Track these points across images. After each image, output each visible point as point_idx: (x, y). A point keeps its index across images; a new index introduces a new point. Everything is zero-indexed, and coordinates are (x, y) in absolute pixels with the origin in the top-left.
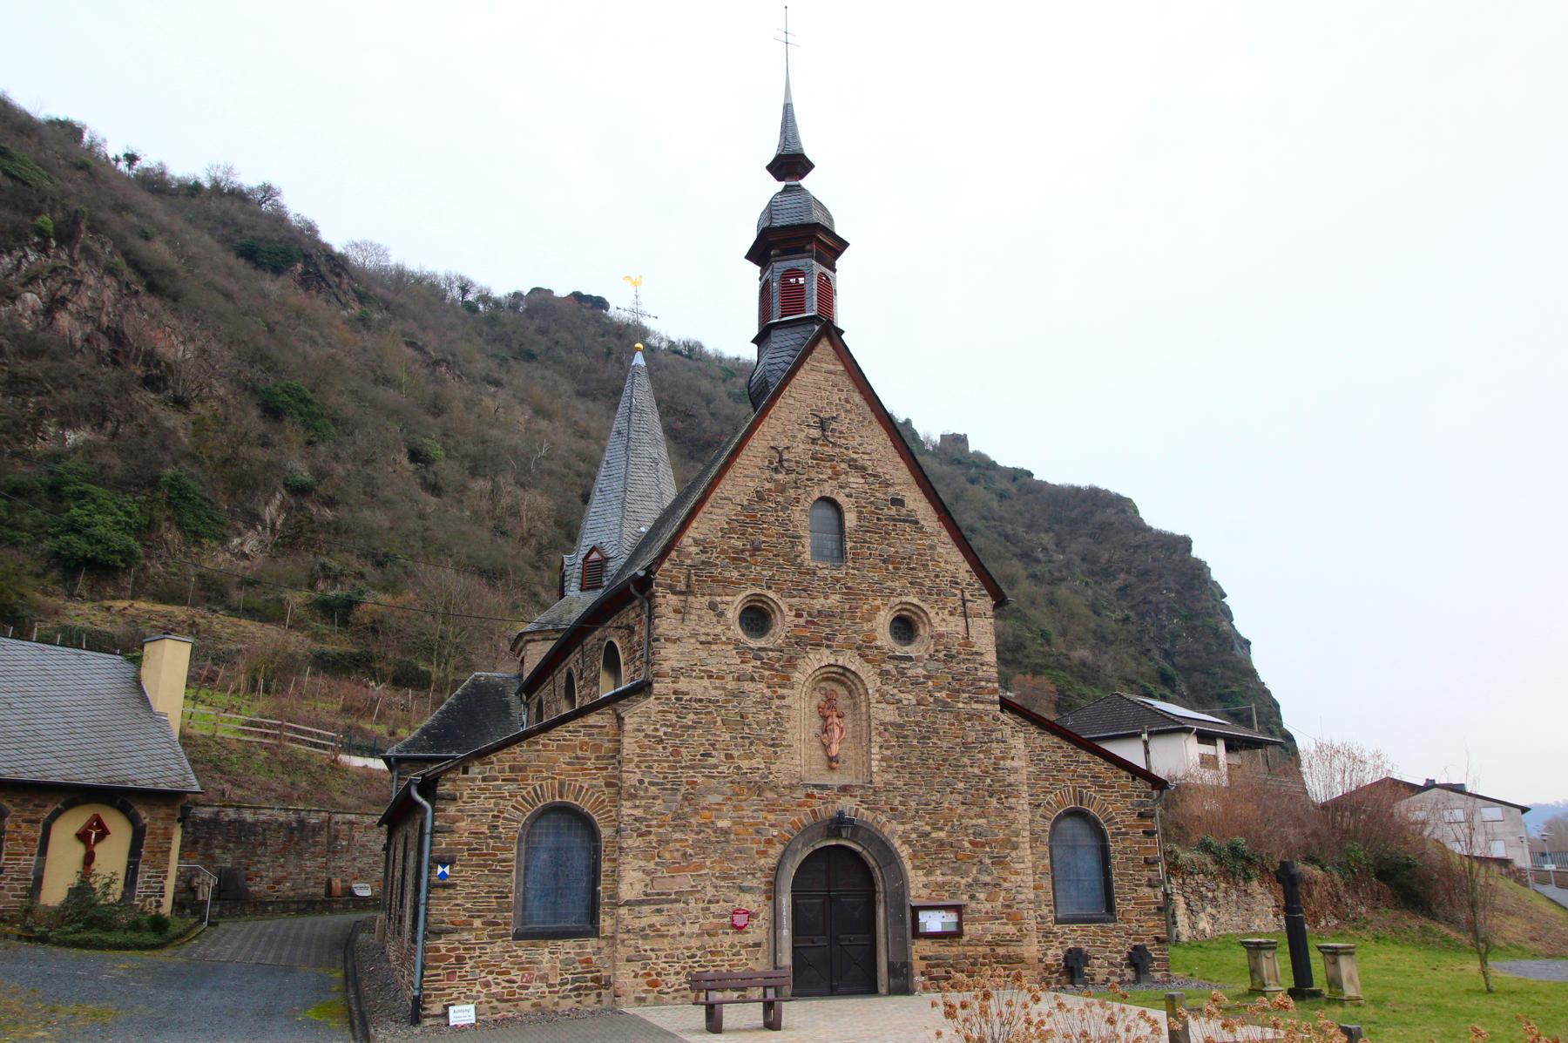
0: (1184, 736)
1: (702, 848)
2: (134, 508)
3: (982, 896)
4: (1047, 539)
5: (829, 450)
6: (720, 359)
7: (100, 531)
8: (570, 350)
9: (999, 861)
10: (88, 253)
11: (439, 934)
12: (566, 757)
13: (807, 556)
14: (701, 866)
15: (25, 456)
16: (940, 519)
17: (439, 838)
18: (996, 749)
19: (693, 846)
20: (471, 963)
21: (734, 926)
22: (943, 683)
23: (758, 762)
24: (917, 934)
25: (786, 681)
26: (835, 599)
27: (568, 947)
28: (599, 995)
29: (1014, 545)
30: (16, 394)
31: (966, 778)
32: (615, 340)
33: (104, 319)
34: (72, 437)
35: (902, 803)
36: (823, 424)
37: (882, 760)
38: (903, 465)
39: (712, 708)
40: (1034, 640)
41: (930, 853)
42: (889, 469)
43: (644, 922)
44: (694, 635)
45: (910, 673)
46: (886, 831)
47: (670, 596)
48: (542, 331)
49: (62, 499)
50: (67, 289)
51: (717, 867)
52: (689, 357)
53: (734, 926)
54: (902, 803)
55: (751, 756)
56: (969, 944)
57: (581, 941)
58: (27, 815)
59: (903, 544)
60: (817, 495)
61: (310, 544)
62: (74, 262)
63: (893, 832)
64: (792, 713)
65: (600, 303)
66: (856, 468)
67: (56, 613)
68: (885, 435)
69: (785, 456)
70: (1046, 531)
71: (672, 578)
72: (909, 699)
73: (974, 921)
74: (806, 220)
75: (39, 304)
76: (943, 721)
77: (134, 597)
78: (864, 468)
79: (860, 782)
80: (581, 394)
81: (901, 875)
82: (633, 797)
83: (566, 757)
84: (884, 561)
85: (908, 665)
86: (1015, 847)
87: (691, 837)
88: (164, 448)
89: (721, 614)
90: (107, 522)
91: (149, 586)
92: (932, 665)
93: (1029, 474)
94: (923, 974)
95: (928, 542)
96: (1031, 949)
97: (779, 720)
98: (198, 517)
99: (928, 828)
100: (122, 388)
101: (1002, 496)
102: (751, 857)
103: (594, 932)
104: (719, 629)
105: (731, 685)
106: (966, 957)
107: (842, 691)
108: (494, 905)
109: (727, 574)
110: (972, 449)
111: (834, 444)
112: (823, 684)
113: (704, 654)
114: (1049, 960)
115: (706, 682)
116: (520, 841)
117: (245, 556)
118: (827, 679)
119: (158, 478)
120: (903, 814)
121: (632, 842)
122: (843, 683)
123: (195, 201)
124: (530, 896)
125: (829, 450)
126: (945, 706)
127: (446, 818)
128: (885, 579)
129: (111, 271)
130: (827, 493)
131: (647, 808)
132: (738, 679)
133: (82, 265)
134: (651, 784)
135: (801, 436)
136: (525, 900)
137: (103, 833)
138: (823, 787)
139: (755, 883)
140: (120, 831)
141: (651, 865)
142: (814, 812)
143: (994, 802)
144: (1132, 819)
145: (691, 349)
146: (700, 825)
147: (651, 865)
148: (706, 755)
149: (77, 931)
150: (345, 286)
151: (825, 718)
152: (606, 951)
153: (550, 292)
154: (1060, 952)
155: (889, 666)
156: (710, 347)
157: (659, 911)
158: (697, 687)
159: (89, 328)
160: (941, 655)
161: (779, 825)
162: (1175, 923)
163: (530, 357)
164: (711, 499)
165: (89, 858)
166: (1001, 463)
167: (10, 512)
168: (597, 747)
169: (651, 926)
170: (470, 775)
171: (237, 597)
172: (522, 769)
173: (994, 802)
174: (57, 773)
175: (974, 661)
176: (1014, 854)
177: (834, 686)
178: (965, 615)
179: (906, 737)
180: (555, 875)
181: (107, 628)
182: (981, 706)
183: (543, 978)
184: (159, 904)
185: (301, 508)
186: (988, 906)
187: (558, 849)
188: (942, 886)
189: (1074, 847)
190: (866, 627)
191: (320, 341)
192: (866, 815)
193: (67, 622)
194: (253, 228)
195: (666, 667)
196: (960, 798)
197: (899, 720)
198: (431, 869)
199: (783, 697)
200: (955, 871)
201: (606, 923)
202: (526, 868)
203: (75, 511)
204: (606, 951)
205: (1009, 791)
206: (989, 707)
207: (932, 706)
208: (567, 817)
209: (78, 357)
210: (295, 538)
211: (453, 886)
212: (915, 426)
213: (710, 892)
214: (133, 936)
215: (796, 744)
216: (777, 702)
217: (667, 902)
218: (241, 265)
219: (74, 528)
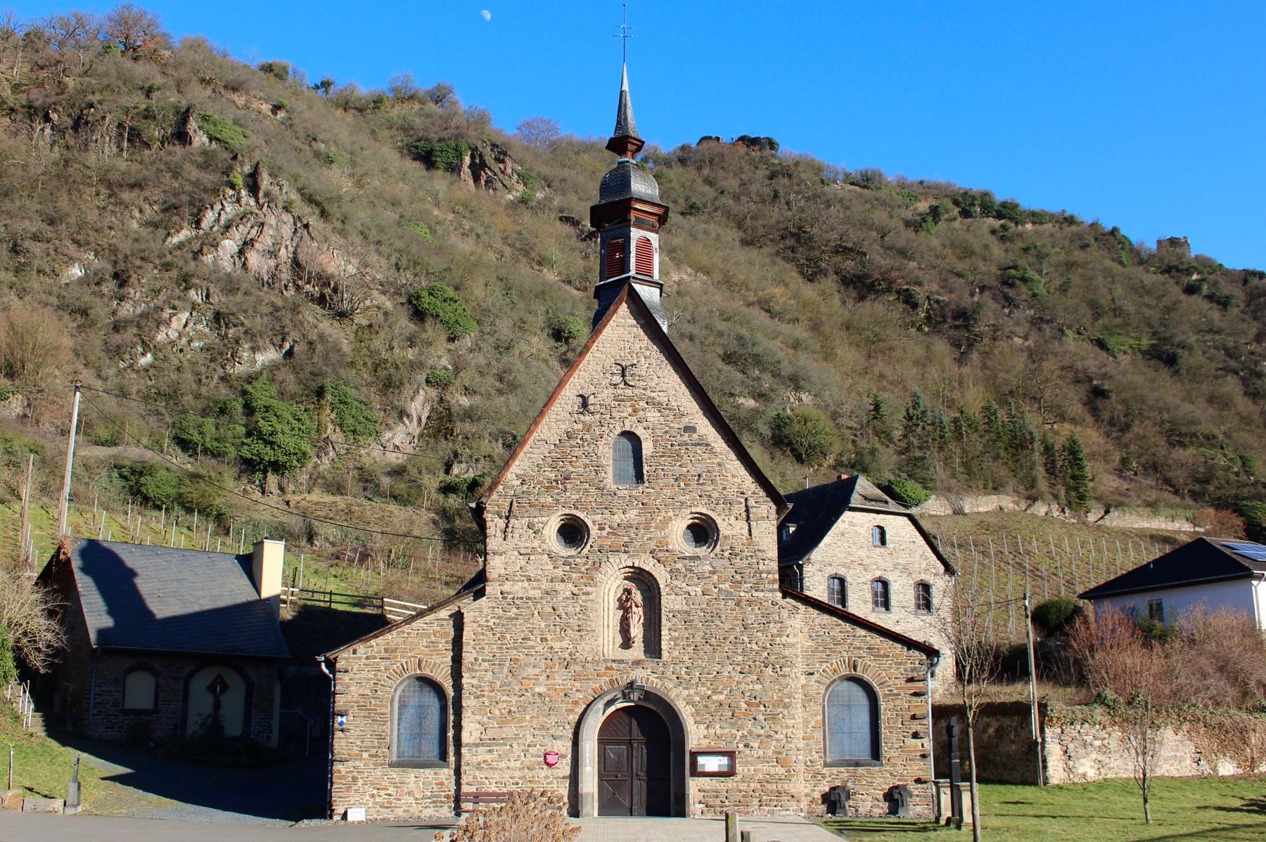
3: (756, 745)
5: (629, 392)
14: (523, 720)
26: (632, 514)
41: (707, 712)
43: (480, 758)
46: (672, 695)
80: (746, 243)
87: (514, 699)
97: (584, 610)
99: (709, 692)
104: (536, 543)
105: (545, 585)
109: (542, 500)
115: (526, 584)
135: (605, 382)
137: (225, 688)
150: (509, 171)
165: (217, 705)
166: (1229, 265)
179: (691, 621)
182: (761, 594)
184: (269, 738)
190: (659, 534)
197: (685, 608)
199: (588, 594)
206: (769, 595)
213: (530, 738)
216: (584, 597)
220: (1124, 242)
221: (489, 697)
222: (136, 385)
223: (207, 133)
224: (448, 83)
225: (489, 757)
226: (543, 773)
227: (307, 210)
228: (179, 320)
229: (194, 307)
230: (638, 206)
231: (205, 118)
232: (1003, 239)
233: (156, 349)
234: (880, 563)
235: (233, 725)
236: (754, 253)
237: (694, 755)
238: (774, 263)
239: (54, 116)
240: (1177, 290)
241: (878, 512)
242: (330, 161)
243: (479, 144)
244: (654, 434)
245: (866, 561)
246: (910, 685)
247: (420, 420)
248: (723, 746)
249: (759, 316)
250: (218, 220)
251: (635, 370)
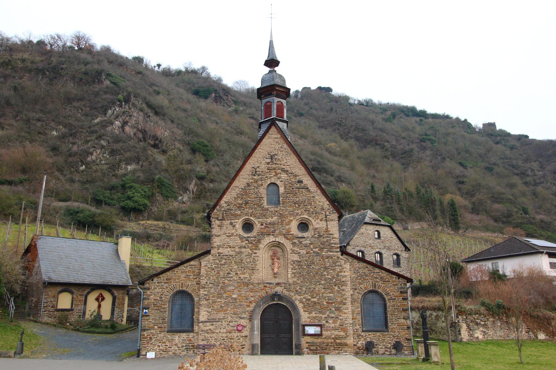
0: (540, 255)
1: (227, 304)
2: (147, 190)
3: (331, 322)
4: (535, 165)
5: (274, 166)
6: (380, 105)
7: (136, 198)
8: (316, 110)
9: (338, 309)
10: (133, 104)
11: (144, 330)
12: (184, 275)
13: (265, 204)
14: (227, 310)
15: (115, 175)
16: (317, 186)
17: (145, 301)
19: (224, 304)
20: (154, 339)
21: (238, 330)
22: (317, 246)
23: (247, 275)
24: (305, 335)
25: (257, 248)
26: (275, 218)
27: (184, 335)
28: (194, 351)
29: (517, 169)
30: (113, 156)
31: (325, 279)
32: (334, 103)
33: (140, 126)
34: (129, 168)
35: (300, 289)
36: (272, 157)
37: (292, 274)
38: (303, 168)
39: (231, 258)
40: (517, 212)
41: (309, 306)
42: (297, 170)
43: (208, 328)
44: (225, 234)
45: (304, 243)
46: (293, 298)
47: (217, 221)
48: (306, 104)
49: (125, 189)
50: (127, 118)
51: (232, 311)
52: (367, 106)
53: (238, 330)
54: (300, 289)
55: (244, 274)
56: (325, 338)
57: (188, 334)
58: (80, 293)
59: (302, 196)
60: (269, 182)
61: (205, 197)
62: (130, 109)
63: (296, 299)
64: (259, 259)
65: (329, 90)
66: (284, 171)
67: (123, 227)
68: (296, 158)
69: (258, 170)
70: (535, 161)
71: (217, 215)
72: (303, 252)
73: (327, 330)
74: (272, 83)
75: (120, 125)
76: (317, 259)
77: (148, 220)
78: (287, 171)
79: (284, 282)
80: (320, 127)
81: (298, 313)
82: (204, 288)
83: (184, 275)
84: (295, 204)
85: (303, 240)
86: (345, 304)
87: (223, 301)
88: (156, 168)
89: (234, 226)
90: (138, 196)
91: (153, 215)
92: (313, 239)
93: (527, 137)
94: (307, 348)
95: (312, 195)
96: (350, 341)
97: (254, 261)
98: (167, 191)
99: (310, 297)
100: (144, 149)
101: (512, 148)
102: (244, 307)
103: (192, 331)
104: (233, 231)
105: (237, 250)
106: (324, 343)
107: (279, 250)
108: (161, 322)
109: (236, 212)
110: (498, 128)
111: (276, 164)
112: (273, 248)
113: (228, 240)
114: (359, 345)
115: (229, 249)
116: (169, 302)
117: (184, 203)
118: (274, 246)
119: (154, 179)
120: (300, 293)
121: (203, 302)
122: (280, 247)
123: (180, 77)
124: (173, 319)
125: (274, 166)
126: (318, 254)
127: (147, 295)
128: (295, 210)
129: (141, 110)
130: (273, 181)
131: (208, 291)
132: (240, 248)
133: (132, 109)
134: (210, 283)
135: (264, 162)
136: (171, 320)
137: (103, 299)
138: (270, 283)
139: (245, 316)
140: (108, 298)
141: (210, 310)
142: (267, 292)
143: (336, 288)
145: (367, 102)
146: (226, 297)
147: (210, 310)
148: (229, 273)
149: (89, 328)
150: (229, 99)
151: (273, 259)
152: (196, 337)
153: (309, 88)
154: (364, 342)
155: (296, 241)
156: (376, 100)
157: (212, 325)
158: (225, 251)
159: (135, 130)
160: (316, 236)
161: (254, 297)
162: (460, 334)
163: (301, 115)
164: (231, 187)
165: (99, 306)
166: (512, 133)
167: (111, 195)
168: (194, 272)
169: (210, 329)
170: (154, 281)
171: (179, 217)
172: (170, 279)
173: (336, 288)
174: (87, 280)
175: (330, 237)
176: (344, 307)
177: (277, 249)
178: (326, 221)
179: (302, 265)
180: (181, 313)
181: (137, 231)
182: (332, 253)
183: (176, 345)
184: (122, 321)
185: (202, 184)
186: (333, 325)
187: (182, 304)
188: (315, 318)
189: (373, 304)
190: (287, 227)
191: (219, 121)
192: (286, 293)
193: (126, 229)
194: (198, 83)
195: (215, 245)
196: (323, 286)
197: (299, 259)
198: (143, 310)
199: (256, 253)
200: (320, 312)
201: (196, 328)
202: (172, 310)
203: (129, 193)
204: (196, 337)
205: (344, 284)
206: (335, 254)
207: (312, 254)
208: (183, 294)
209: (132, 141)
210: (200, 195)
211: (148, 316)
212: (469, 121)
213: (230, 319)
214: (104, 330)
215: (261, 269)
216: (254, 255)
217: (215, 322)
218: (193, 98)
219: (129, 198)
220: (469, 125)
221: (212, 300)
222: (77, 178)
223: (109, 80)
225: (211, 327)
226: (235, 335)
227: (149, 111)
228: (96, 152)
229: (103, 147)
231: (109, 75)
232: (420, 124)
233: (87, 164)
234: (378, 246)
235: (106, 315)
236: (323, 131)
237: (304, 326)
238: (331, 135)
240: (491, 143)
241: (377, 225)
242: (158, 93)
244: (285, 185)
245: (372, 245)
248: (317, 323)
249: (326, 154)
250: (113, 114)
251: (276, 157)
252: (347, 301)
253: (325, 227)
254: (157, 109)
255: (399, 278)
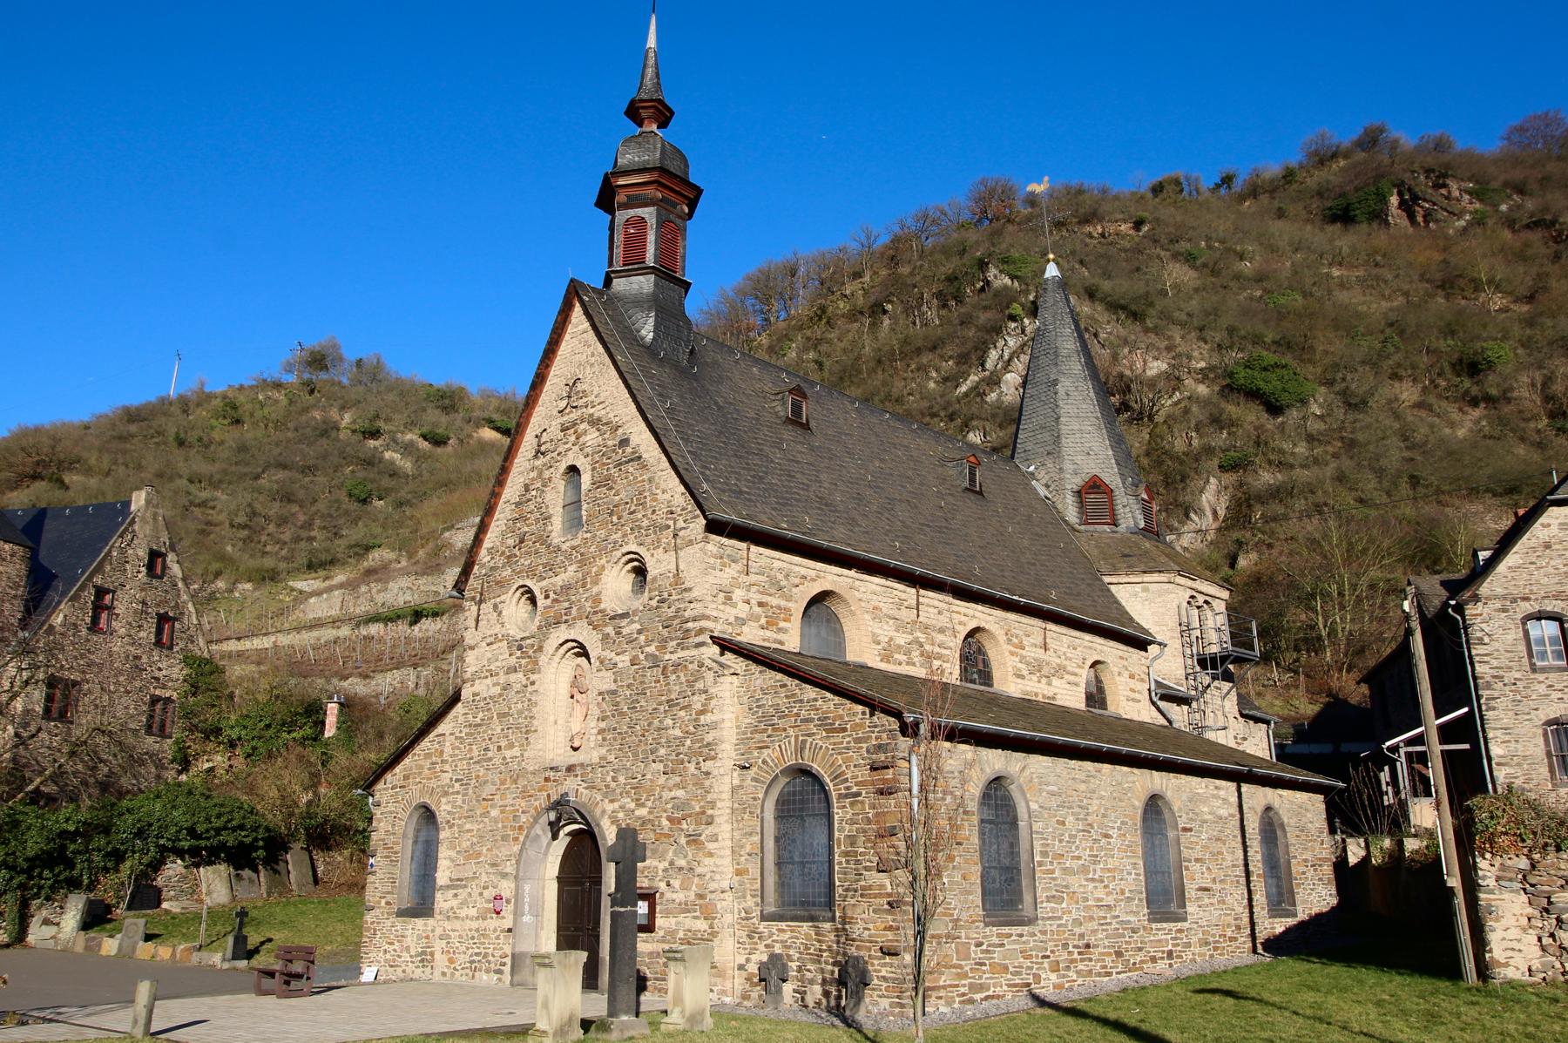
18: (697, 702)
46: (598, 812)
63: (604, 812)
73: (667, 913)
85: (624, 622)
105: (502, 679)
144: (864, 774)
150: (1456, 193)
197: (613, 687)
213: (484, 878)
224: (1377, 123)
230: (621, 182)
239: (889, 307)
243: (1407, 177)
246: (877, 776)
247: (1215, 513)
250: (1002, 356)
252: (716, 812)
253: (673, 567)
254: (1133, 307)
255: (872, 715)
